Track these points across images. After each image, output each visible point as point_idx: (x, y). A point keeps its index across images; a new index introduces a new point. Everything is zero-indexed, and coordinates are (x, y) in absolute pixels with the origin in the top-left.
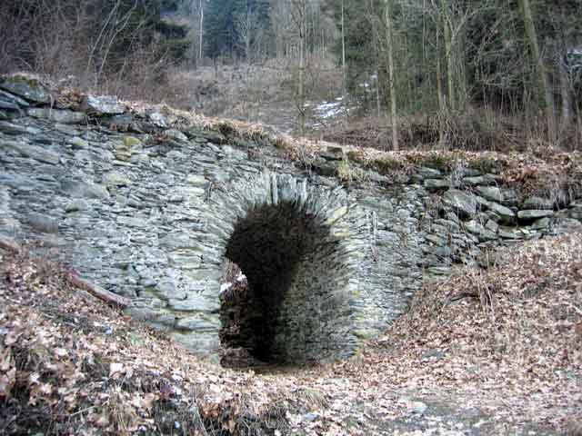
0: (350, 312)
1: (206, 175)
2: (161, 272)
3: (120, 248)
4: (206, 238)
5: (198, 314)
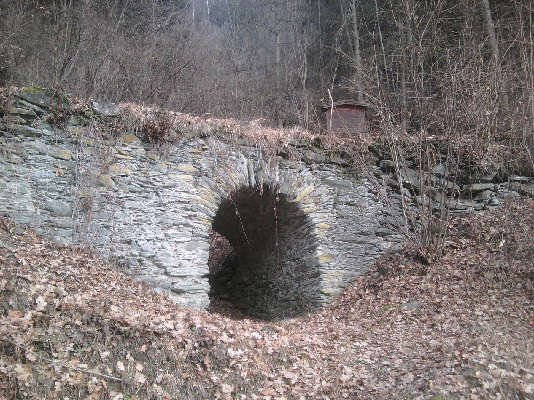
2: (159, 245)
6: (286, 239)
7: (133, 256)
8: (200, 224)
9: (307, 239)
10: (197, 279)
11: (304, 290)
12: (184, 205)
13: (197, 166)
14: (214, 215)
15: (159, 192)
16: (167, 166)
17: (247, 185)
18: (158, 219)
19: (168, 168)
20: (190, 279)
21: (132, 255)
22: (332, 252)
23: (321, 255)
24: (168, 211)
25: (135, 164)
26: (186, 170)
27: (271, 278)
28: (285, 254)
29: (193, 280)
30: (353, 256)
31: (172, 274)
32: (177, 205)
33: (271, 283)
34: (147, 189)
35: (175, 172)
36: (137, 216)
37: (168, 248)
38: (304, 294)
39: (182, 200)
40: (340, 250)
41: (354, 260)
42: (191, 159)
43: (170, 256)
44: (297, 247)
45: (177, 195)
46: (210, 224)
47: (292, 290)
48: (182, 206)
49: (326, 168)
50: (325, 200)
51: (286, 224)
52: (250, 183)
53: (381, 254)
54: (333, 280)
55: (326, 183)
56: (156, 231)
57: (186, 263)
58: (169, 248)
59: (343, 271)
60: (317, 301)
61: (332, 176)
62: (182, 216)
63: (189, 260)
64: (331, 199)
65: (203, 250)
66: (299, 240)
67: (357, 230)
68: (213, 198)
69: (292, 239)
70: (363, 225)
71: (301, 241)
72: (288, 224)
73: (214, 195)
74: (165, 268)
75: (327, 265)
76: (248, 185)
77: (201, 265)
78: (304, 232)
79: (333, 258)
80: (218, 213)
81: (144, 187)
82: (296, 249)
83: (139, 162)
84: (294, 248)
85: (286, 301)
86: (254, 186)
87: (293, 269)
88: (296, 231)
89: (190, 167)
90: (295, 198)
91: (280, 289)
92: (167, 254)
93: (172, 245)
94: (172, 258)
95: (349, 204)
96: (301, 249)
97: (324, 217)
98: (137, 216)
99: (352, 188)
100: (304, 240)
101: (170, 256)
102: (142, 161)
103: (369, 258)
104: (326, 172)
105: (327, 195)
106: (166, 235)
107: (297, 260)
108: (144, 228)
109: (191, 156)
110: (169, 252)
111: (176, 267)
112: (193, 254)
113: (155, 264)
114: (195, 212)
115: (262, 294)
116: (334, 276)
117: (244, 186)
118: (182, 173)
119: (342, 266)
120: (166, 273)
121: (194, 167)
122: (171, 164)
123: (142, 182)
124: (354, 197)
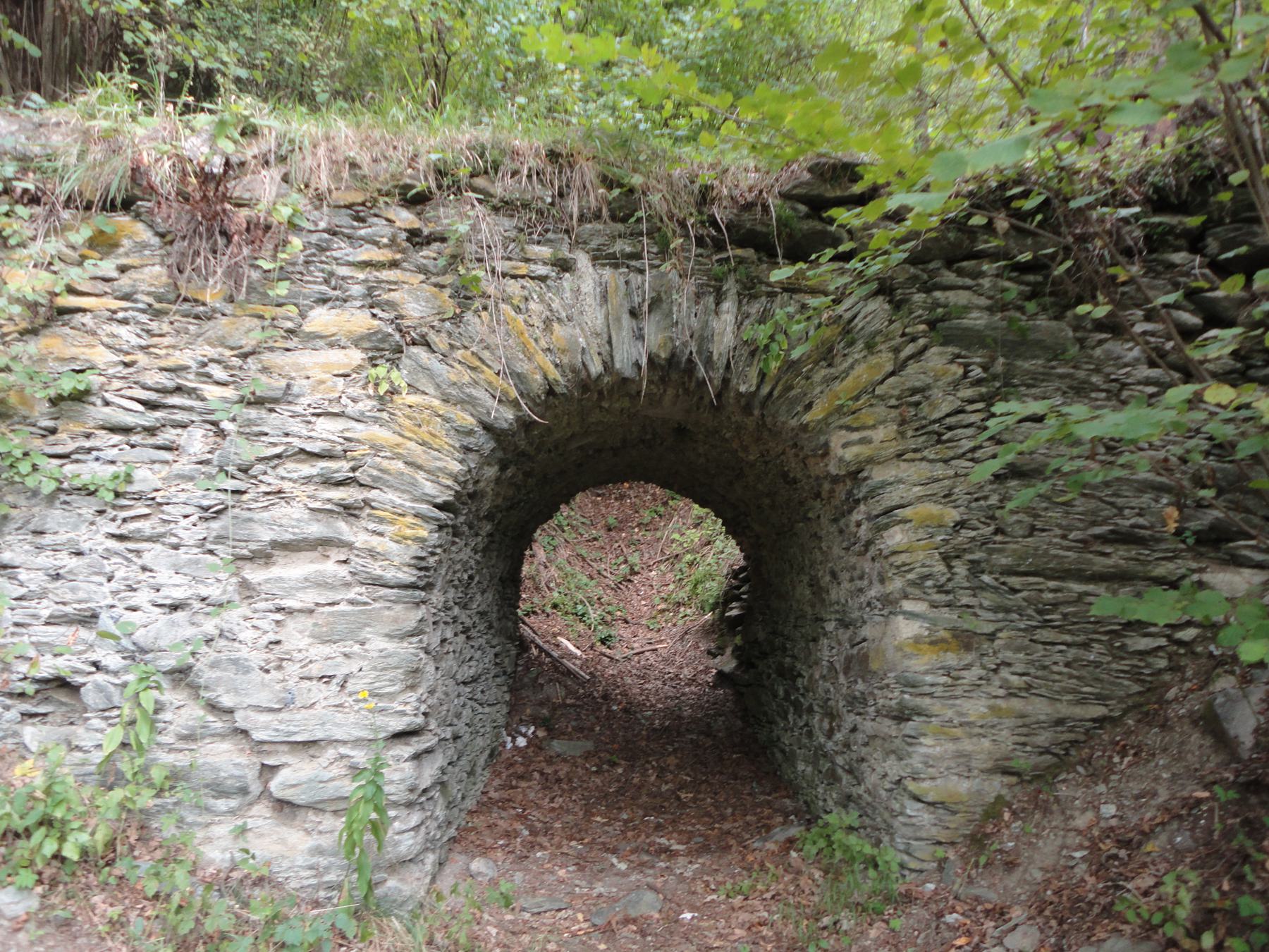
0: (901, 716)
1: (372, 302)
2: (210, 627)
3: (74, 562)
4: (367, 502)
5: (331, 753)
8: (381, 534)
22: (969, 623)
26: (333, 330)
37: (241, 637)
39: (309, 447)
41: (1072, 653)
42: (357, 290)
43: (247, 670)
45: (296, 426)
48: (314, 471)
49: (949, 277)
50: (945, 408)
54: (967, 745)
57: (319, 692)
59: (1016, 703)
61: (979, 308)
63: (326, 679)
65: (390, 636)
70: (1120, 501)
79: (968, 647)
83: (143, 318)
89: (359, 320)
92: (235, 662)
97: (937, 480)
99: (1074, 350)
101: (247, 670)
103: (1144, 643)
108: (150, 565)
110: (244, 652)
112: (346, 655)
118: (321, 343)
119: (1015, 680)
123: (157, 391)
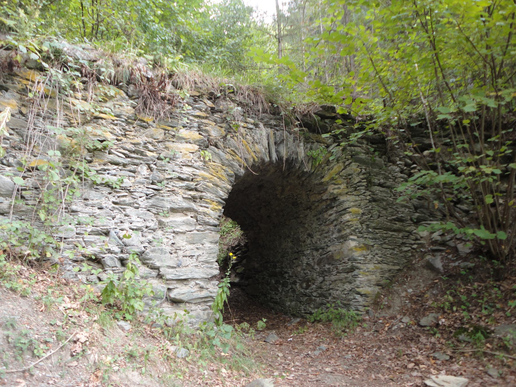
2: (150, 237)
6: (306, 226)
7: (112, 253)
8: (207, 208)
9: (336, 226)
10: (202, 284)
11: (331, 287)
12: (186, 182)
13: (203, 134)
14: (226, 196)
15: (152, 166)
16: (163, 131)
17: (267, 159)
18: (150, 201)
19: (165, 134)
20: (193, 283)
21: (110, 251)
23: (356, 247)
24: (164, 191)
25: (118, 127)
26: (189, 137)
27: (287, 268)
28: (304, 241)
29: (197, 284)
30: (390, 247)
31: (169, 277)
32: (176, 182)
33: (286, 273)
34: (136, 161)
35: (174, 140)
36: (118, 197)
38: (331, 291)
39: (182, 176)
40: (376, 239)
42: (196, 125)
44: (321, 235)
46: (221, 208)
47: (313, 284)
50: (357, 181)
51: (307, 209)
52: (270, 157)
53: (418, 244)
55: (356, 161)
56: (146, 218)
57: (188, 261)
58: (165, 240)
59: (380, 265)
60: (351, 303)
62: (184, 198)
63: (192, 256)
64: (363, 179)
65: (211, 242)
66: (323, 227)
67: (392, 216)
68: (225, 178)
69: (314, 225)
70: (398, 209)
71: (326, 229)
72: (310, 208)
73: (225, 171)
74: (158, 269)
75: (363, 258)
76: (269, 159)
77: (208, 263)
78: (333, 217)
79: (368, 249)
80: (232, 194)
81: (132, 157)
82: (319, 237)
83: (124, 124)
84: (317, 236)
85: (306, 295)
86: (275, 162)
87: (316, 260)
88: (320, 216)
89: (194, 135)
90: (323, 177)
91: (298, 281)
92: (162, 250)
93: (169, 236)
94: (168, 255)
95: (380, 185)
96: (326, 237)
98: (118, 197)
99: (384, 166)
100: (332, 227)
101: (165, 253)
102: (128, 123)
103: (406, 249)
104: (356, 148)
105: (359, 174)
106: (160, 223)
107: (321, 250)
109: (196, 120)
110: (164, 247)
111: (173, 268)
112: (197, 248)
113: (144, 264)
114: (202, 192)
115: (276, 284)
116: (370, 271)
117: (263, 160)
118: (184, 141)
120: (160, 276)
121: (199, 134)
122: (170, 128)
123: (129, 151)
124: (387, 178)
